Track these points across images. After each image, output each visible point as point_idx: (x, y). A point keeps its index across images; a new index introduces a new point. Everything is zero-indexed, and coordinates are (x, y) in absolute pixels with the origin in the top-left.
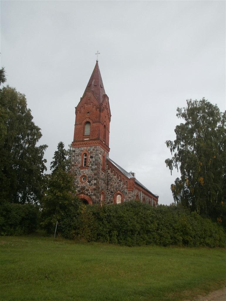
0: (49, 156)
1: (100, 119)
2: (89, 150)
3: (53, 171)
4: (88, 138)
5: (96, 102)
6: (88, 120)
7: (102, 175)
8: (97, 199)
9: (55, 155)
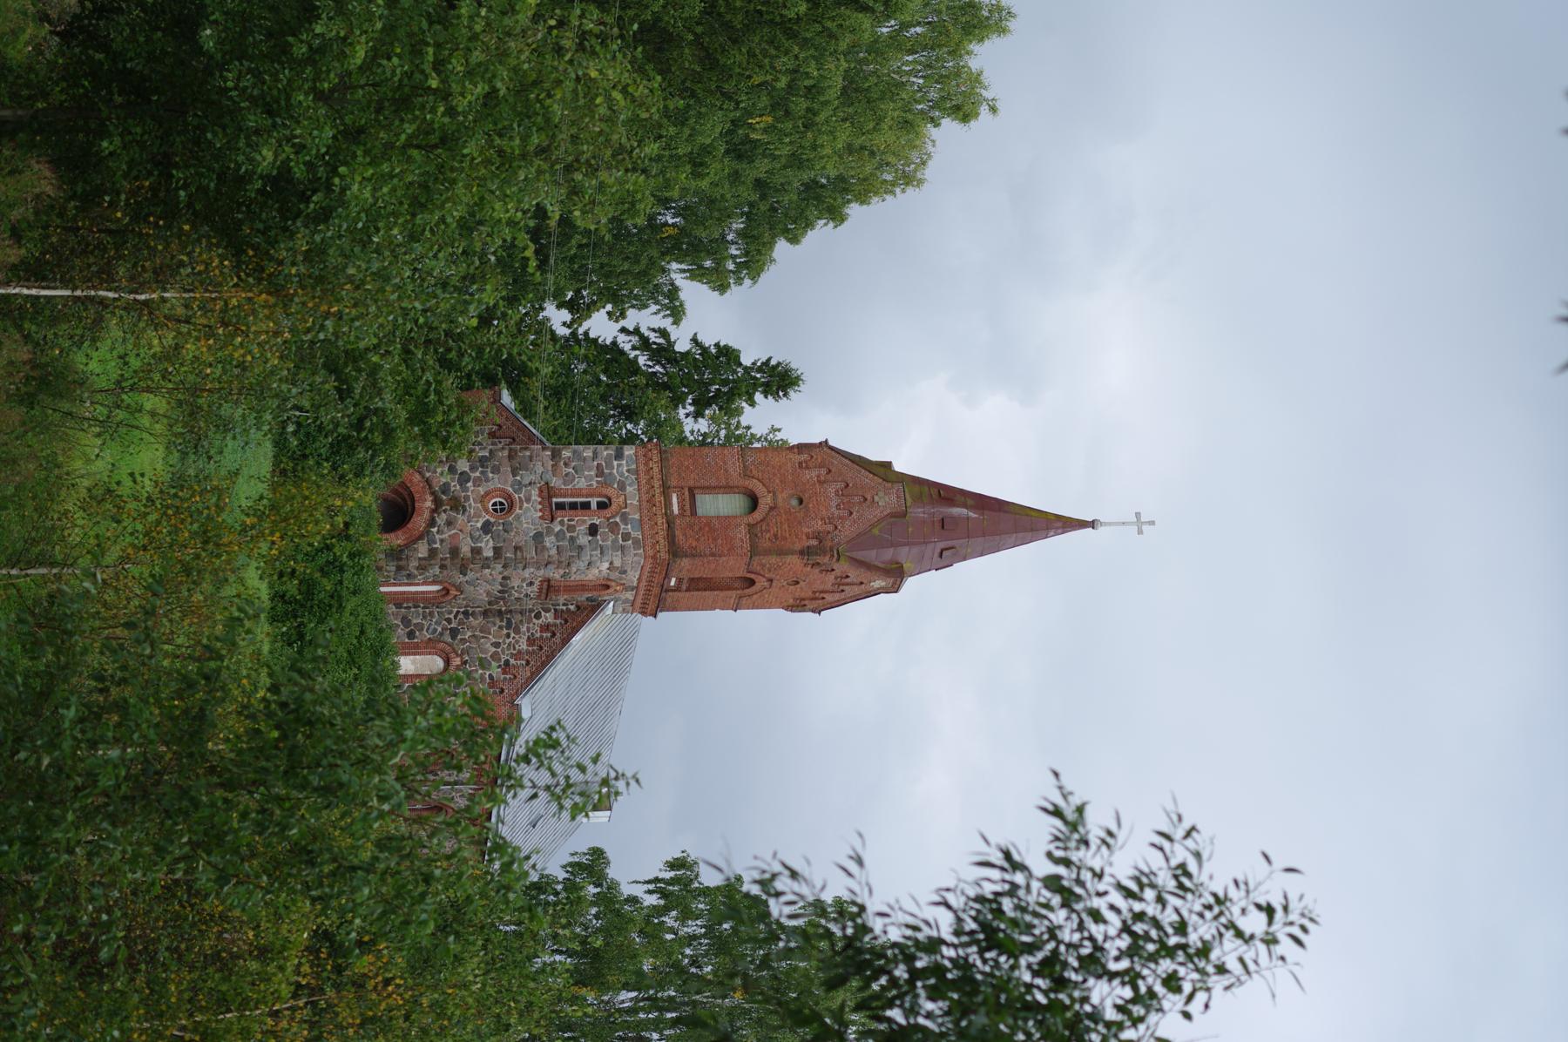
0: (708, 316)
1: (768, 552)
2: (624, 518)
3: (614, 343)
4: (681, 508)
5: (848, 530)
6: (765, 501)
7: (525, 582)
8: (414, 563)
9: (717, 345)
